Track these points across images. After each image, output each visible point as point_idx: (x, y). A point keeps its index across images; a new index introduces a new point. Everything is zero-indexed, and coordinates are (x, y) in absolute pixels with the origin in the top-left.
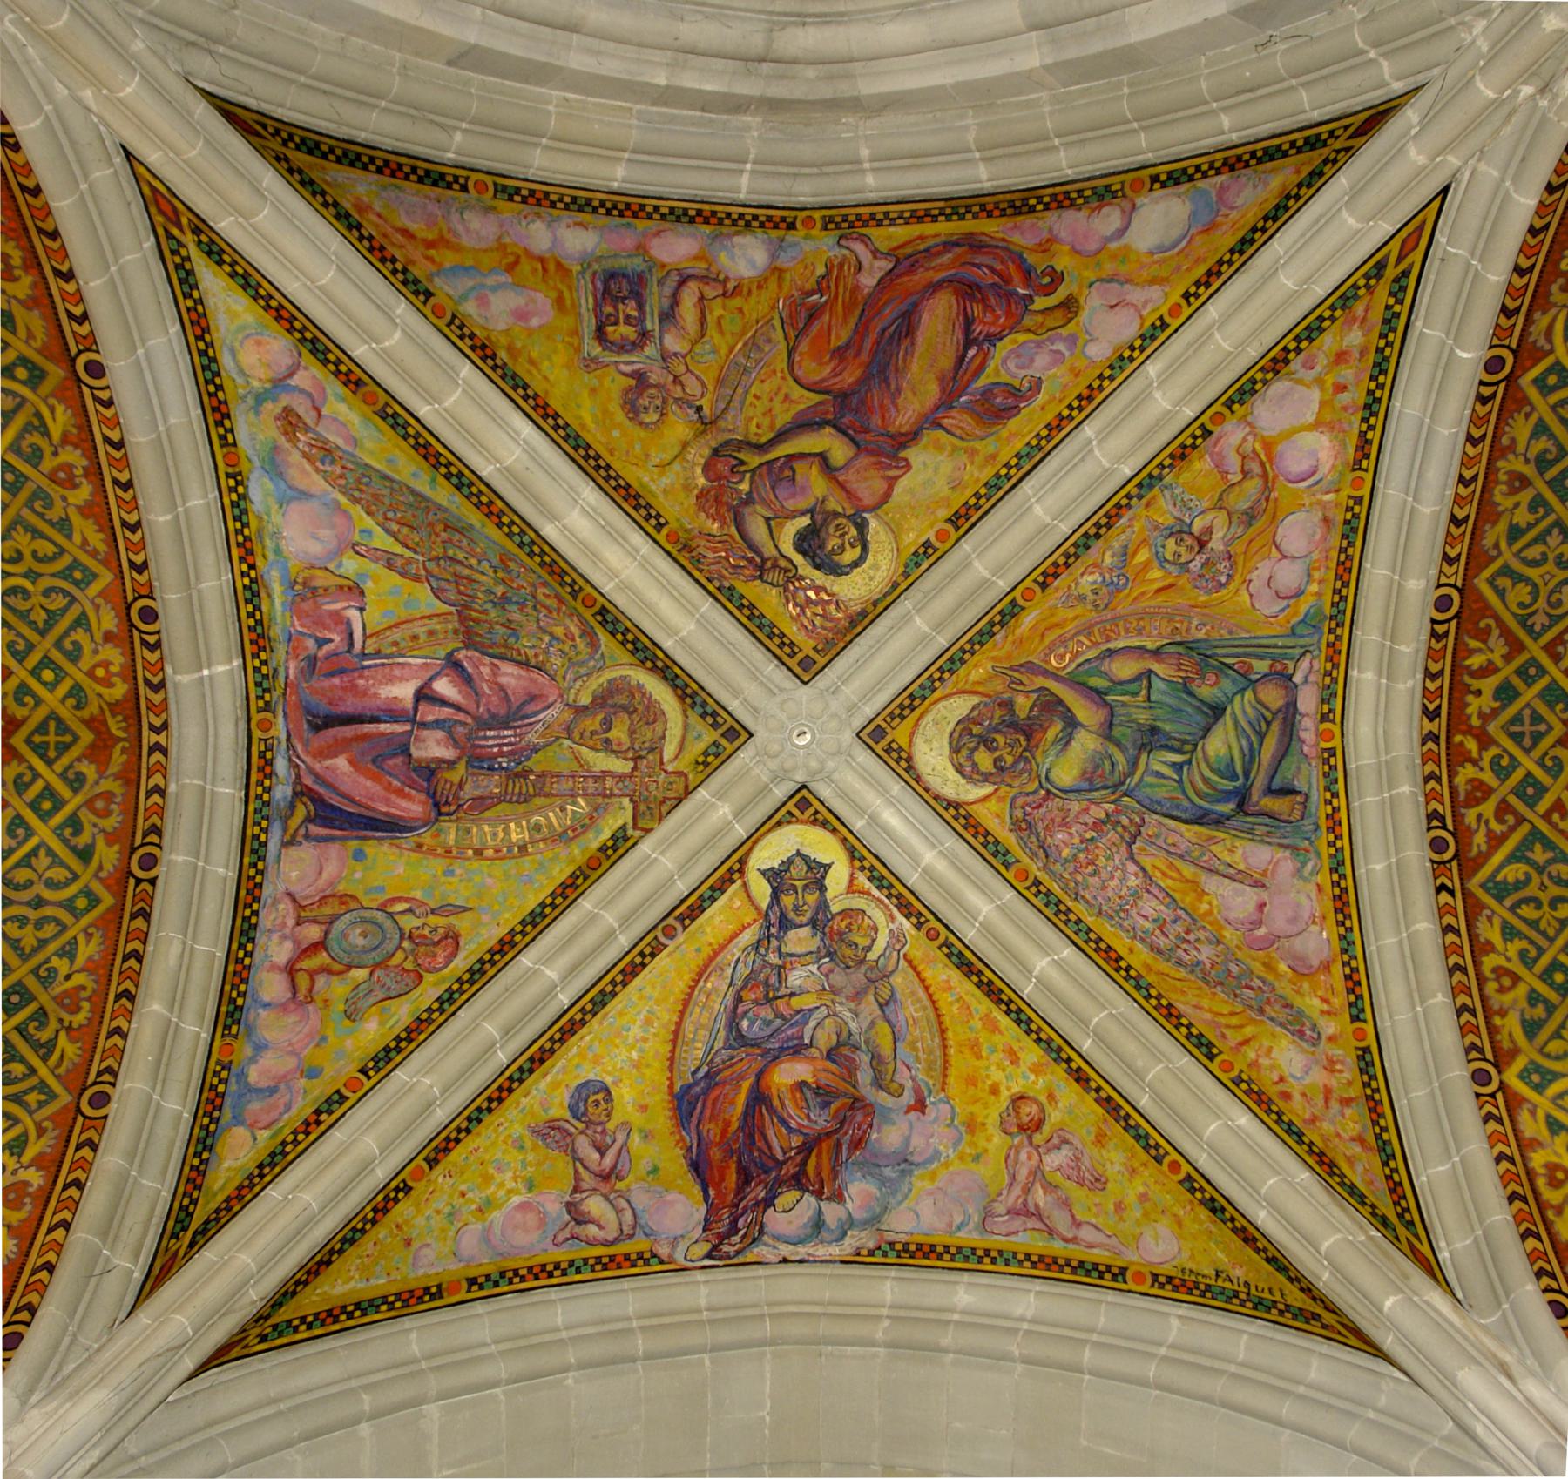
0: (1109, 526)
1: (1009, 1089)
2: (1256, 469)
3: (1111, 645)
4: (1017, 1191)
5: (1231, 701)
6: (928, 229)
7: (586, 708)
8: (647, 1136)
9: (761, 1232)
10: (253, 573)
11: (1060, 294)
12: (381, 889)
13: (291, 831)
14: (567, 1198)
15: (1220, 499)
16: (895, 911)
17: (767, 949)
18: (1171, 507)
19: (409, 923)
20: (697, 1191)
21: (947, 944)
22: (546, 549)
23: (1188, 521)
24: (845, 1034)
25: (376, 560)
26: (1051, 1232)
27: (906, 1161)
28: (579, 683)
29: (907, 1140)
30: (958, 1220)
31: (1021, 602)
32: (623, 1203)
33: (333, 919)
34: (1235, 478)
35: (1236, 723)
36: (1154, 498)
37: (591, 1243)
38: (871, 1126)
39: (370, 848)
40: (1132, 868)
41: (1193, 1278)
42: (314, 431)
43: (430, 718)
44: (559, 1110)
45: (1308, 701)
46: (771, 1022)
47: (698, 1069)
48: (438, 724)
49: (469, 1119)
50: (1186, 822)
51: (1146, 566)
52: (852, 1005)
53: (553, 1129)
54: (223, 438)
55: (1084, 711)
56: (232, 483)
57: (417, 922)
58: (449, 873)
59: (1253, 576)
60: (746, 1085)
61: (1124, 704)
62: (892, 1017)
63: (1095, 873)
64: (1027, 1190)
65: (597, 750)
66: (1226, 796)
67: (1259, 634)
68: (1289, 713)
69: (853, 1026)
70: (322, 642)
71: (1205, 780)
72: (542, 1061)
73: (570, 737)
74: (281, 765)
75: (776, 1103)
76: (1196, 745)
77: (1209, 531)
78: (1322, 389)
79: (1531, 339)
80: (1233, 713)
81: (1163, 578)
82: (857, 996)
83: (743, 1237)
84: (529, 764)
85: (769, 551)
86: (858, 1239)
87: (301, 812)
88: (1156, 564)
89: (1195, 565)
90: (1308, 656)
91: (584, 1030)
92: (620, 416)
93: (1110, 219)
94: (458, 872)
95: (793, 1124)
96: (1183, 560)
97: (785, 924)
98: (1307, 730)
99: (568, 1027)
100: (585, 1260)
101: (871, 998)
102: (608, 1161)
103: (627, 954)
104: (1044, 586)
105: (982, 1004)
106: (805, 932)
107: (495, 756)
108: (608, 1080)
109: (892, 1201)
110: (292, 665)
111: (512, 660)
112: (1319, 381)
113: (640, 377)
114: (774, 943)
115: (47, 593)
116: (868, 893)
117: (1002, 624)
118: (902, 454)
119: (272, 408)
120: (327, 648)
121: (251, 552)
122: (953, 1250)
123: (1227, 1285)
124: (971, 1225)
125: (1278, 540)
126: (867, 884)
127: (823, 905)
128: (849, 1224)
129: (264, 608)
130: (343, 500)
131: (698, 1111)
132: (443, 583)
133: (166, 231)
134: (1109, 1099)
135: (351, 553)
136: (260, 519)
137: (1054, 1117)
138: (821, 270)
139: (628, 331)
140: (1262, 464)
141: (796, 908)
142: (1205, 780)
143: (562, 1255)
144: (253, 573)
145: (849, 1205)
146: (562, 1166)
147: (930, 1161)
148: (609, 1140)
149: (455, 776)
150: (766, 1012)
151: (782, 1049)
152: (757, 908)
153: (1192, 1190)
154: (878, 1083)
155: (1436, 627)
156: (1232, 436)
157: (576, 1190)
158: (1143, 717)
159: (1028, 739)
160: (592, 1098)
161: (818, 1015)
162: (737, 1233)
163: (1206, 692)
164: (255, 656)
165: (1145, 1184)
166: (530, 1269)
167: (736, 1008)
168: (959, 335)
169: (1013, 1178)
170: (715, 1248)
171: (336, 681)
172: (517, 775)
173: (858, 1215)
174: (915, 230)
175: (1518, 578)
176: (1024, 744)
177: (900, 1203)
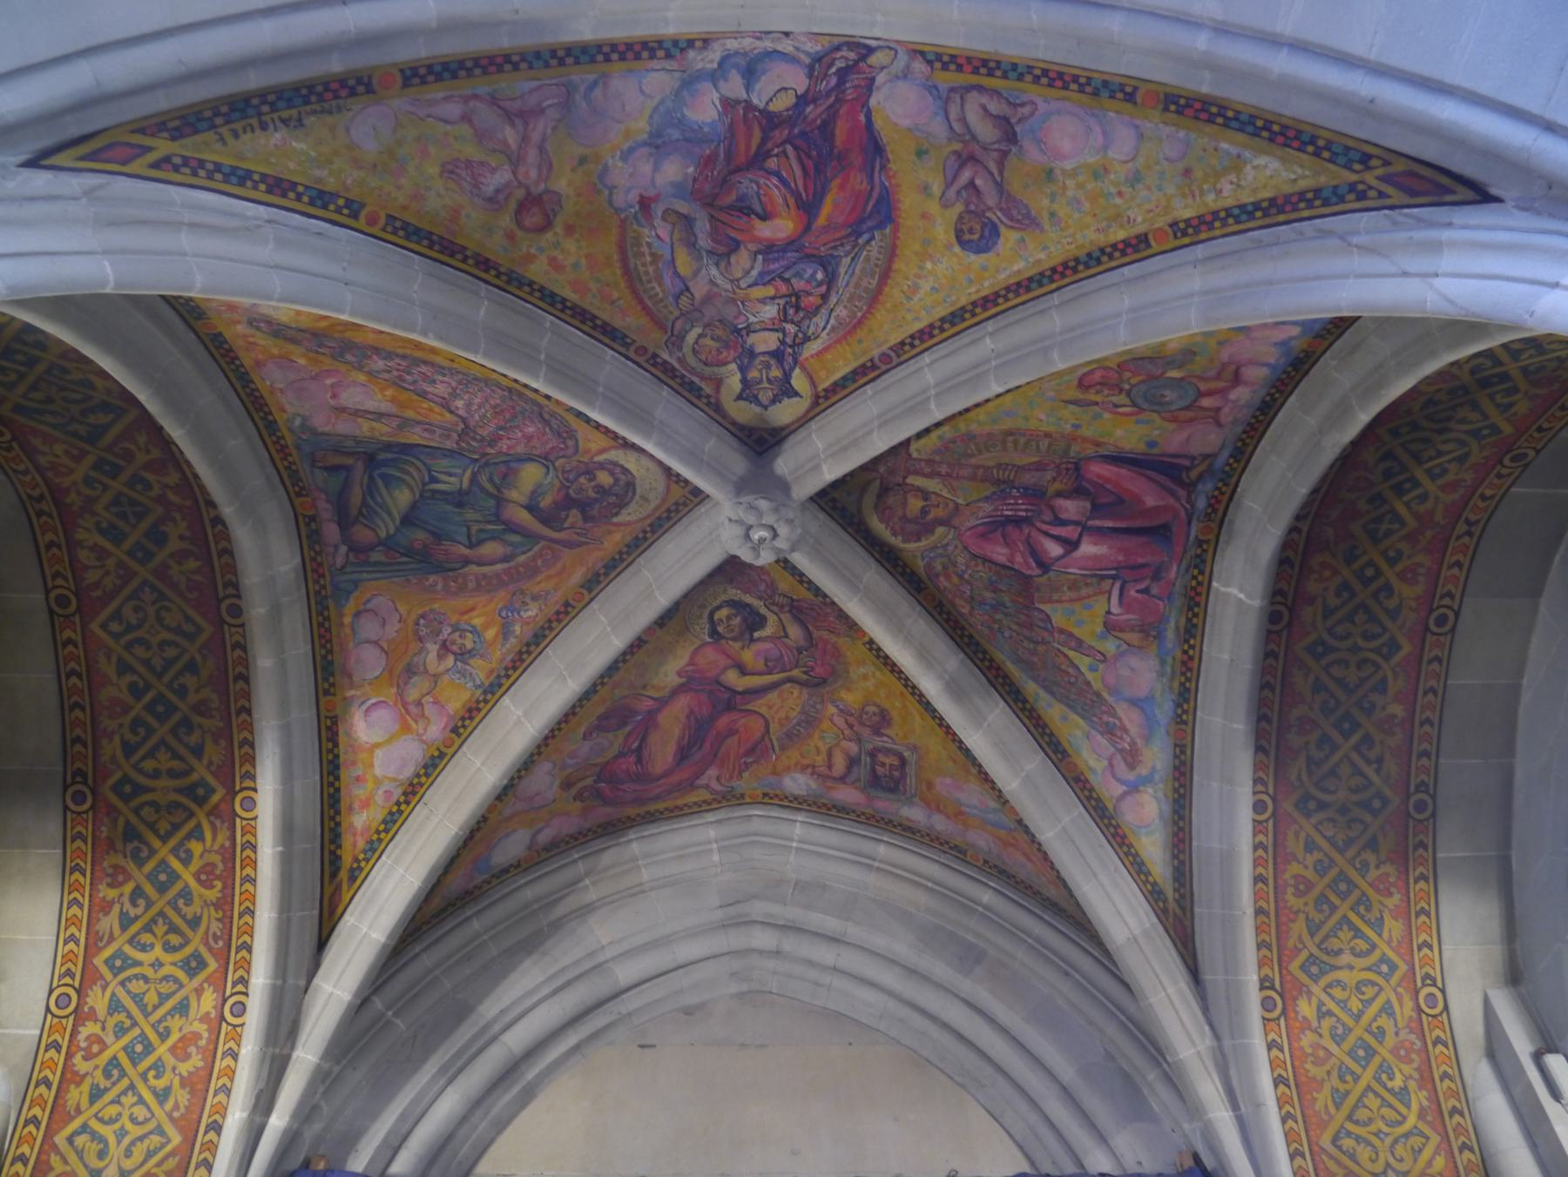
0: (520, 653)
1: (556, 234)
2: (414, 710)
3: (505, 565)
4: (535, 137)
5: (397, 529)
6: (670, 804)
7: (940, 524)
8: (925, 189)
9: (811, 68)
10: (1186, 647)
11: (574, 791)
12: (1137, 422)
13: (1207, 463)
14: (1014, 149)
15: (436, 682)
16: (677, 365)
17: (796, 336)
18: (474, 672)
19: (1121, 399)
20: (878, 123)
21: (628, 346)
22: (958, 640)
23: (459, 663)
24: (723, 265)
25: (1091, 647)
26: (494, 101)
27: (657, 147)
28: (946, 541)
29: (656, 169)
30: (598, 92)
31: (584, 591)
32: (957, 127)
33: (1187, 408)
34: (429, 699)
35: (389, 513)
36: (488, 677)
37: (995, 93)
38: (695, 180)
39: (1142, 447)
40: (462, 412)
41: (326, 105)
42: (1117, 749)
43: (1070, 528)
44: (1008, 238)
45: (331, 531)
46: (795, 275)
47: (868, 242)
48: (1064, 523)
49: (1099, 262)
50: (418, 445)
51: (487, 626)
52: (715, 290)
53: (1018, 221)
54: (1183, 752)
55: (524, 517)
56: (1184, 717)
57: (1113, 399)
58: (1077, 427)
59: (398, 626)
60: (821, 220)
61: (489, 522)
62: (677, 281)
63: (495, 407)
64: (525, 139)
65: (934, 493)
66: (385, 463)
67: (384, 582)
68: (344, 521)
69: (714, 271)
70: (1146, 591)
71: (408, 473)
72: (1019, 284)
73: (957, 504)
74: (1201, 503)
75: (791, 201)
76: (421, 496)
77: (440, 657)
78: (375, 778)
79: (226, 824)
80: (393, 520)
81: (471, 618)
82: (709, 299)
83: (830, 66)
84: (993, 489)
85: (786, 617)
86: (708, 60)
87: (1194, 474)
88: (479, 629)
89: (446, 631)
90: (338, 566)
91: (974, 297)
92: (894, 714)
93: (543, 838)
94: (1068, 426)
95: (775, 180)
96: (457, 634)
97: (777, 355)
98: (325, 509)
99: (989, 305)
100: (1005, 76)
101: (697, 295)
102: (966, 175)
103: (927, 349)
104: (567, 604)
105: (591, 303)
106: (760, 348)
107: (1020, 497)
108: (957, 249)
109: (669, 104)
110: (1173, 575)
111: (997, 564)
112: (378, 782)
113: (877, 731)
114: (789, 340)
115: (1349, 635)
116: (702, 378)
117: (598, 574)
118: (682, 680)
119: (1143, 771)
120: (1142, 586)
121: (1184, 663)
122: (600, 58)
123: (285, 114)
124: (582, 89)
125: (383, 655)
126: (703, 385)
127: (743, 369)
128: (715, 77)
129: (1183, 620)
130: (1105, 695)
131: (871, 204)
132: (1042, 625)
133: (1185, 914)
134: (452, 255)
135: (1108, 656)
136: (1171, 688)
137: (506, 220)
138: (746, 775)
139: (881, 757)
140: (408, 712)
141: (768, 367)
142: (408, 473)
143: (1030, 91)
144: (1186, 647)
145: (716, 96)
146: (1015, 185)
147: (631, 150)
148: (964, 193)
149: (1057, 486)
150: (798, 284)
151: (784, 251)
152: (803, 369)
153: (349, 203)
154: (687, 221)
155: (234, 592)
156: (435, 730)
157: (1005, 154)
158: (470, 515)
159: (567, 494)
160: (976, 237)
161: (750, 280)
162: (839, 70)
163: (420, 535)
164: (1200, 584)
165: (399, 188)
166: (1065, 87)
167: (829, 290)
168: (645, 753)
169: (541, 149)
170: (863, 58)
171: (1141, 560)
172: (1004, 482)
173: (706, 86)
174: (679, 802)
175: (178, 630)
176: (571, 491)
177: (662, 102)
